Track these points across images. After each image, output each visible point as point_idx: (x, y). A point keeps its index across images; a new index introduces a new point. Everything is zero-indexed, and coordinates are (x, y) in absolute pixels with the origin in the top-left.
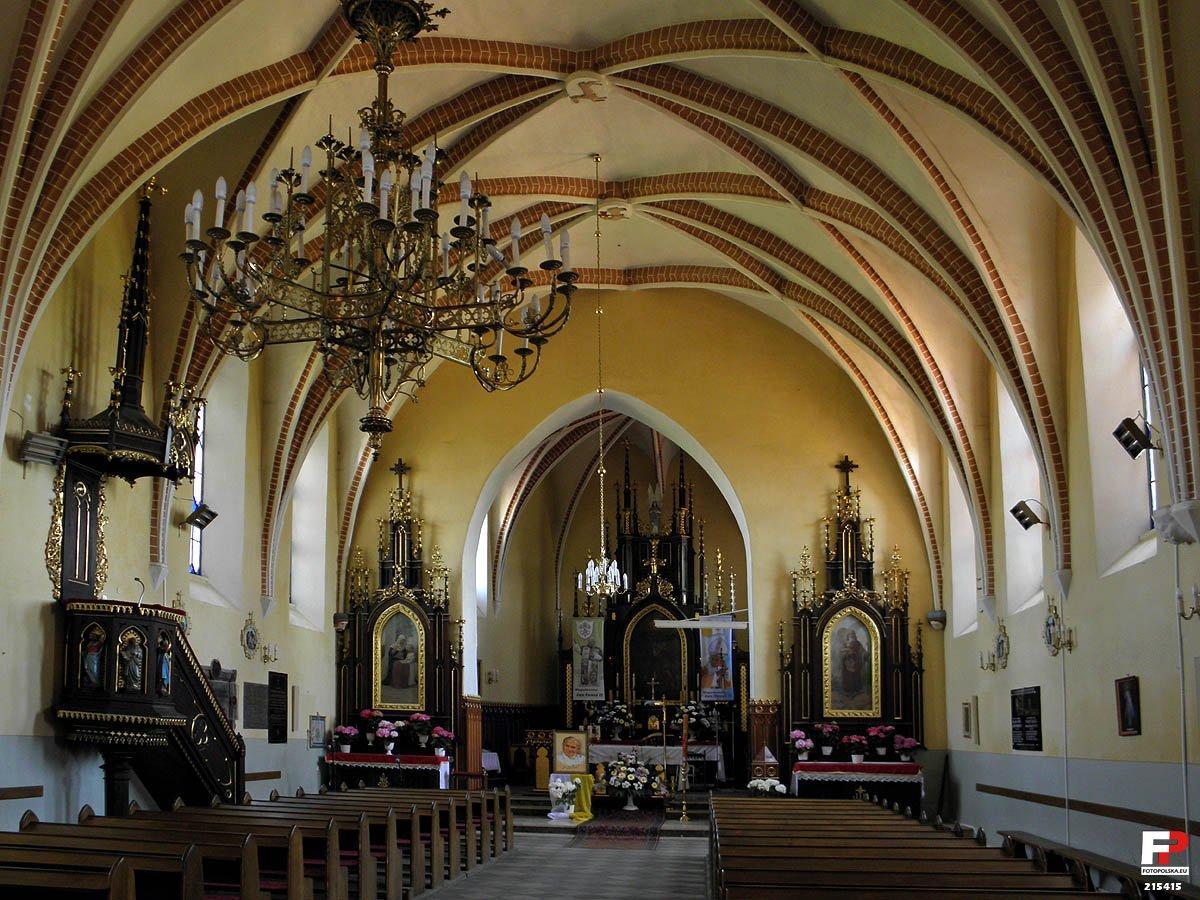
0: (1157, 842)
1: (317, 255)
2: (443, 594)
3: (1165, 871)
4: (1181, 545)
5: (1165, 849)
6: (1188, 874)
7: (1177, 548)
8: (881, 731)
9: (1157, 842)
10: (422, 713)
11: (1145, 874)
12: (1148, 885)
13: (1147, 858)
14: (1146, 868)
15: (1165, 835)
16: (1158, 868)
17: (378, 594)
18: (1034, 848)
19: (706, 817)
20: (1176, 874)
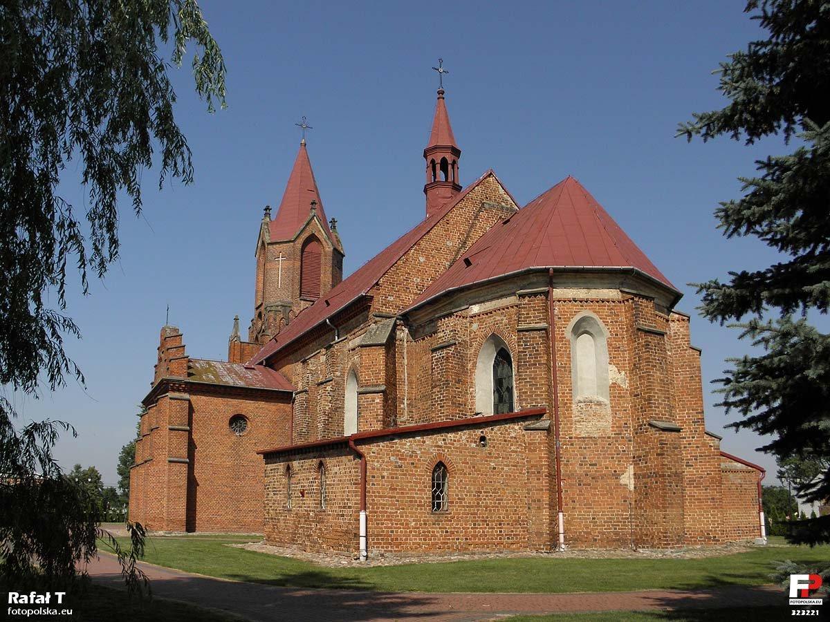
0: (800, 582)
1: (272, 314)
2: (579, 404)
3: (806, 602)
4: (382, 351)
5: (806, 587)
6: (821, 604)
7: (381, 345)
8: (497, 556)
9: (800, 582)
10: (45, 597)
11: (792, 604)
12: (794, 611)
13: (793, 593)
14: (792, 600)
15: (806, 577)
16: (801, 600)
17: (545, 490)
18: (128, 512)
19: (799, 596)
20: (813, 604)
